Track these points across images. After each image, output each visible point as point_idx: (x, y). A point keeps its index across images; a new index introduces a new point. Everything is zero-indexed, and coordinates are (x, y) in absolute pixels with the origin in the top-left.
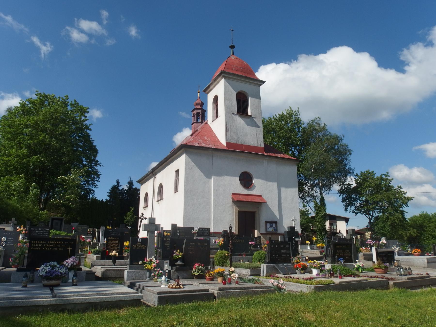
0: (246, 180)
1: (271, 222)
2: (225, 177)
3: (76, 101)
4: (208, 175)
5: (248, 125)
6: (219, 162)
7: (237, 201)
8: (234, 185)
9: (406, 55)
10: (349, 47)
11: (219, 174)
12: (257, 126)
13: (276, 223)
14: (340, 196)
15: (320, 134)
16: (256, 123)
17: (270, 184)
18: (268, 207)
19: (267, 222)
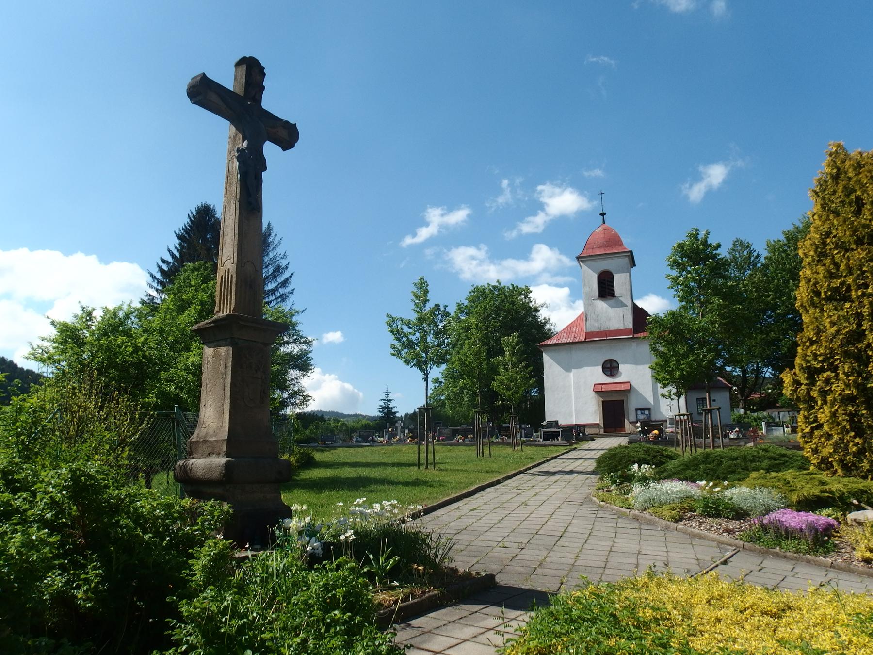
0: (611, 368)
1: (643, 410)
2: (586, 368)
3: (512, 285)
4: (568, 369)
5: (612, 307)
6: (577, 354)
7: (599, 392)
8: (596, 375)
9: (428, 220)
10: (44, 249)
11: (579, 366)
12: (623, 305)
13: (649, 409)
14: (708, 233)
15: (721, 281)
16: (622, 302)
17: (641, 367)
18: (638, 394)
19: (637, 410)
